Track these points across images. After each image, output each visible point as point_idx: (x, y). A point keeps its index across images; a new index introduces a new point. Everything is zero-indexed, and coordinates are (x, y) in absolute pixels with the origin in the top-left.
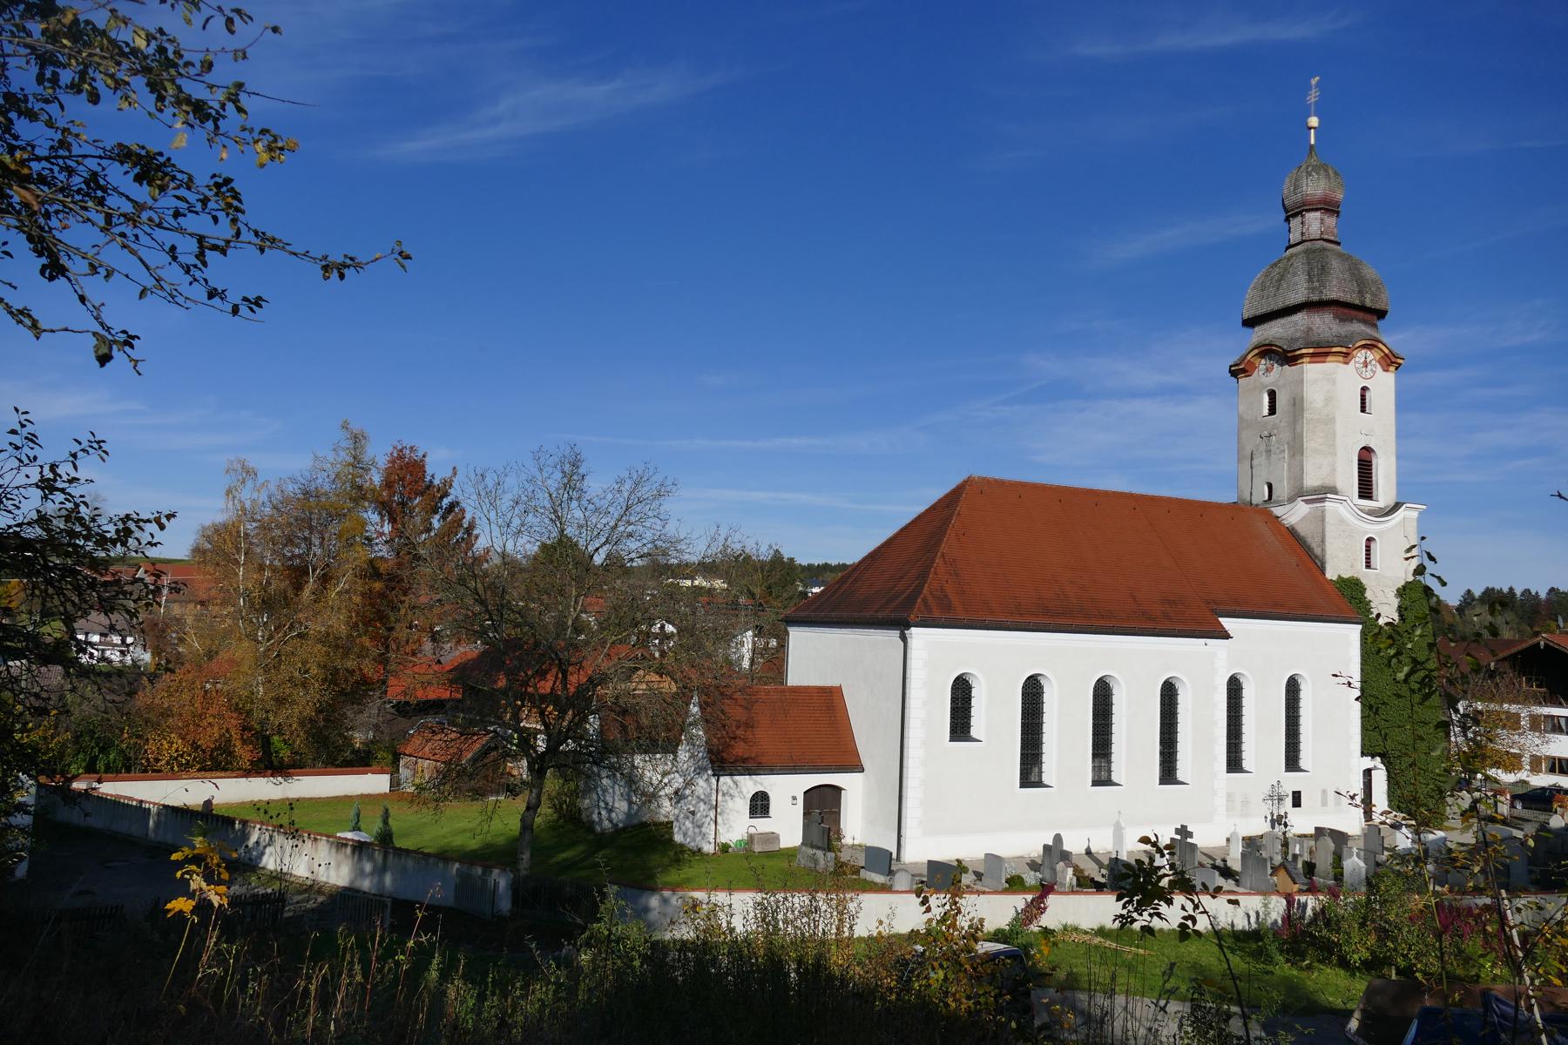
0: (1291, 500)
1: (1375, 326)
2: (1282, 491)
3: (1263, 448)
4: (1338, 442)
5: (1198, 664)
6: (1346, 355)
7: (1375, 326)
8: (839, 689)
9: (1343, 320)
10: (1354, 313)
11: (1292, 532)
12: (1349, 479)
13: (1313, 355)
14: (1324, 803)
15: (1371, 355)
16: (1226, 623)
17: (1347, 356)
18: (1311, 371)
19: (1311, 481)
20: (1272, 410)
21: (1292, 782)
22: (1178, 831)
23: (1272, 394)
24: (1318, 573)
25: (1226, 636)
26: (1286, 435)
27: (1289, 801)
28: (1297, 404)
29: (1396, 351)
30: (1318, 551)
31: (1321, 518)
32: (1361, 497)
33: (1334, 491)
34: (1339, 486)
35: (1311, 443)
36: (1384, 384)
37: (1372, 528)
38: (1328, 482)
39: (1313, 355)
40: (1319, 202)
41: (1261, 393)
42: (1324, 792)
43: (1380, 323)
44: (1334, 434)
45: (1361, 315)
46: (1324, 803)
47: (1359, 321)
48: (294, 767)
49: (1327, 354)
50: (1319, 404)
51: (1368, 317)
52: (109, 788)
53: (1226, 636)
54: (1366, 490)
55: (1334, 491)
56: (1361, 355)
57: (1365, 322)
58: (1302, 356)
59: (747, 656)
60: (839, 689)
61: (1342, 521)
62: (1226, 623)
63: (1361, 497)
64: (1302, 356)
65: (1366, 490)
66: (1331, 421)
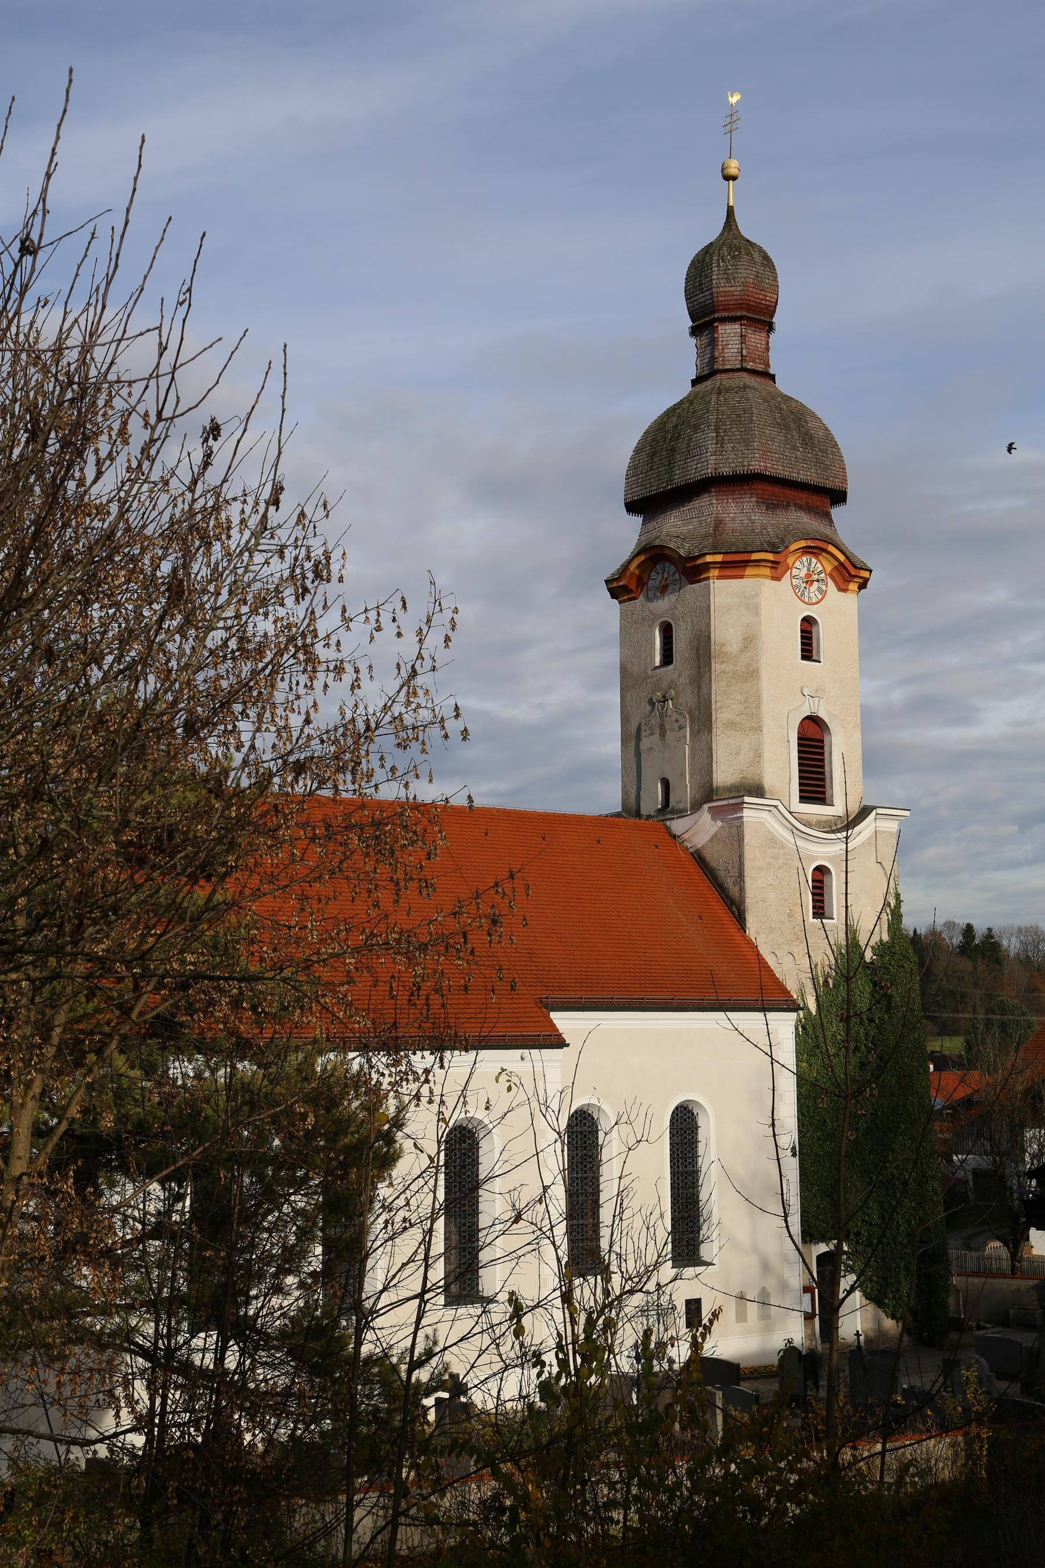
0: (696, 807)
2: (685, 791)
3: (655, 720)
4: (765, 709)
6: (775, 565)
7: (827, 517)
9: (772, 506)
10: (791, 493)
11: (699, 858)
12: (782, 769)
13: (723, 565)
15: (818, 565)
16: (563, 1021)
17: (777, 570)
18: (722, 591)
19: (724, 775)
20: (667, 658)
23: (667, 631)
24: (732, 927)
25: (559, 1043)
26: (687, 698)
28: (703, 650)
30: (734, 891)
31: (736, 838)
32: (803, 799)
33: (758, 791)
34: (768, 782)
35: (726, 706)
37: (825, 851)
39: (723, 565)
40: (740, 306)
41: (651, 627)
43: (836, 512)
44: (758, 697)
45: (804, 497)
47: (800, 507)
49: (745, 564)
50: (733, 646)
51: (816, 500)
52: (721, 1435)
53: (559, 1043)
54: (814, 785)
55: (758, 791)
57: (809, 509)
58: (707, 566)
61: (773, 841)
62: (563, 1021)
63: (803, 799)
64: (707, 566)
65: (814, 785)
66: (752, 674)
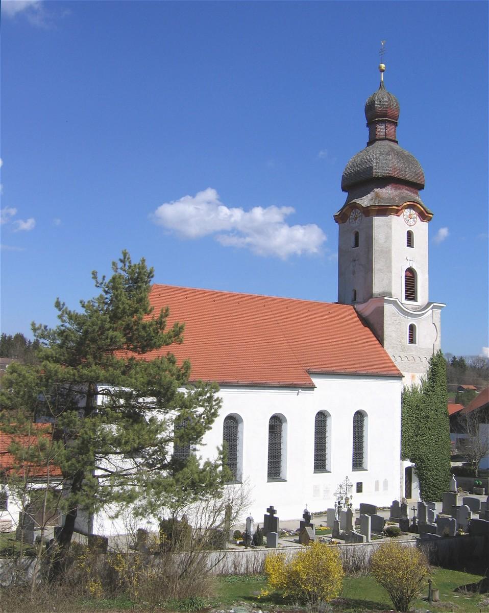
1: (417, 193)
5: (298, 408)
8: (360, 504)
12: (398, 289)
14: (377, 489)
16: (316, 381)
20: (357, 245)
21: (358, 476)
22: (268, 510)
27: (355, 488)
29: (428, 210)
32: (407, 299)
36: (421, 229)
38: (386, 290)
42: (377, 483)
43: (420, 192)
46: (377, 489)
48: (390, 279)
56: (407, 212)
59: (477, 473)
60: (360, 504)
63: (407, 299)
